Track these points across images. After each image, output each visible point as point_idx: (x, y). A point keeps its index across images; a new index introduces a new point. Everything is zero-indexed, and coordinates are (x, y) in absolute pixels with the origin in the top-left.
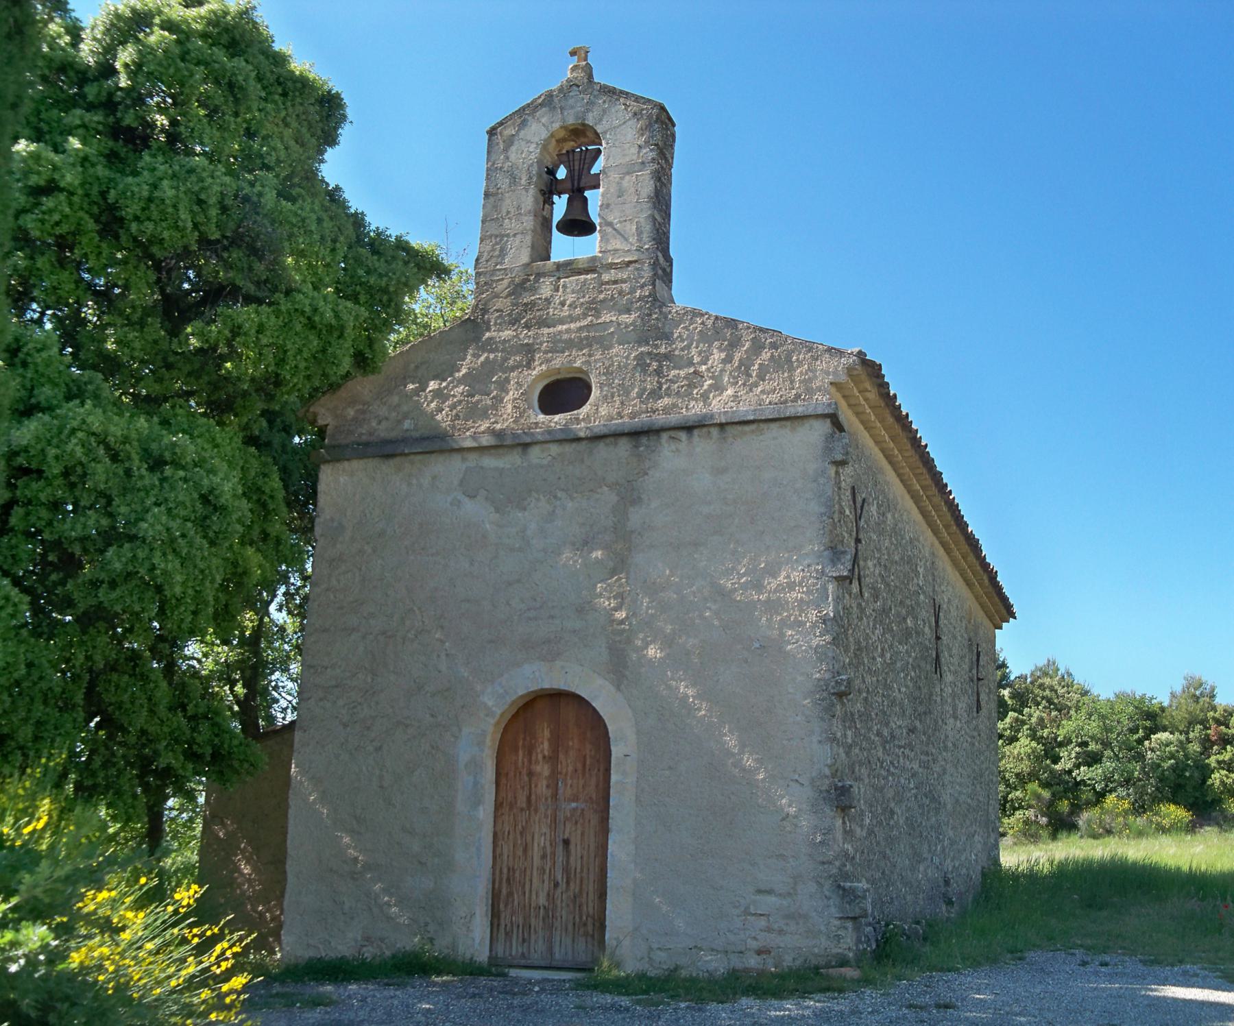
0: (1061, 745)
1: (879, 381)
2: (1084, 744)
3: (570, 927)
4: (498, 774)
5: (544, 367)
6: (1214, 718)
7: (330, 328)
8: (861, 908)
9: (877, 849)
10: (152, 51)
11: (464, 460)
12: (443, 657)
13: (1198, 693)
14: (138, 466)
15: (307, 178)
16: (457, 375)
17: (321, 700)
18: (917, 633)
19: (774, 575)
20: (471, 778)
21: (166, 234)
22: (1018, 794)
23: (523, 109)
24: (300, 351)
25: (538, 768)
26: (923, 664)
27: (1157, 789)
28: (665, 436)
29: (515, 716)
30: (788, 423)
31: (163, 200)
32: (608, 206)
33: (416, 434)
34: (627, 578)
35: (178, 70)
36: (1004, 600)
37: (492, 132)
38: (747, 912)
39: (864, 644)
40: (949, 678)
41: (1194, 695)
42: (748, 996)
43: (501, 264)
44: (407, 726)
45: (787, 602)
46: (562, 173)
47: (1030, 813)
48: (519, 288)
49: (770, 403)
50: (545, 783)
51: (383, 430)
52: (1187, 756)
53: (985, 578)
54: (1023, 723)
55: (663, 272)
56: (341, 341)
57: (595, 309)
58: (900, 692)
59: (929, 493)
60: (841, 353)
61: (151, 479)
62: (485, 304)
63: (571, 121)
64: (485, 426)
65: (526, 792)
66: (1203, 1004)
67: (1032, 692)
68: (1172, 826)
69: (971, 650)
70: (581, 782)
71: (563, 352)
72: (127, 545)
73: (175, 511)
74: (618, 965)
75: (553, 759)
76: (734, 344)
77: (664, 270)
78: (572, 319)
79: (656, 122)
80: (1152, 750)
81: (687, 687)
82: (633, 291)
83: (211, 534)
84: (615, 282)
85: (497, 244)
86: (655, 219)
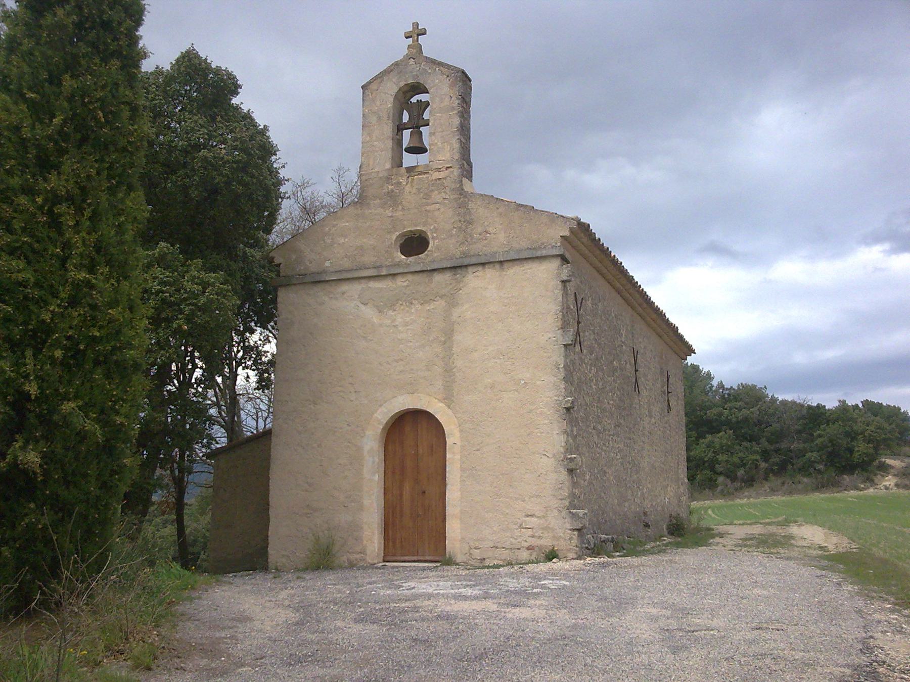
40: (644, 393)
46: (406, 117)
55: (467, 171)
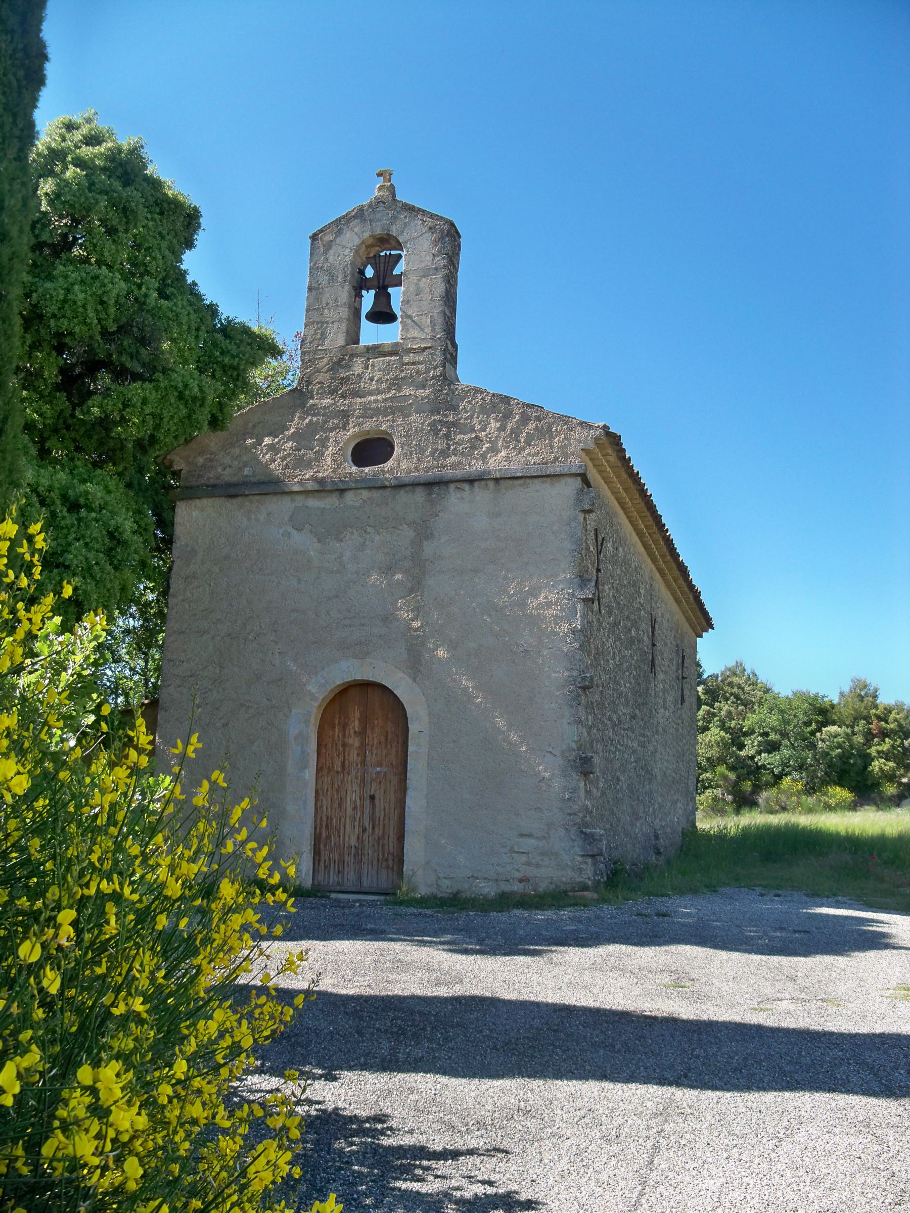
0: (746, 734)
1: (618, 448)
2: (766, 734)
3: (375, 863)
4: (319, 745)
5: (356, 429)
6: (876, 715)
7: (194, 399)
8: (598, 848)
9: (607, 806)
10: (67, 183)
11: (293, 500)
12: (277, 654)
13: (863, 694)
14: (61, 510)
15: (177, 279)
16: (286, 433)
17: (179, 686)
18: (639, 641)
19: (536, 596)
20: (299, 748)
21: (77, 329)
22: (708, 775)
23: (339, 219)
24: (172, 417)
25: (351, 741)
26: (642, 666)
27: (826, 773)
28: (452, 486)
29: (332, 701)
30: (549, 479)
31: (75, 302)
32: (408, 302)
33: (253, 480)
34: (422, 596)
35: (87, 199)
36: (705, 614)
37: (314, 238)
38: (512, 851)
39: (601, 650)
40: (661, 676)
41: (860, 695)
42: (518, 908)
43: (322, 345)
44: (248, 707)
45: (545, 617)
46: (369, 272)
47: (718, 792)
48: (337, 365)
49: (534, 463)
50: (356, 752)
51: (227, 476)
52: (852, 747)
53: (691, 596)
54: (714, 715)
55: (450, 357)
56: (203, 409)
57: (397, 384)
58: (625, 687)
59: (651, 531)
60: (590, 427)
61: (70, 519)
62: (309, 378)
63: (378, 231)
64: (309, 474)
65: (341, 759)
66: (847, 918)
67: (722, 689)
68: (837, 805)
69: (677, 654)
70: (385, 752)
71: (372, 418)
72: (55, 571)
73: (92, 545)
74: (414, 889)
75: (362, 734)
76: (507, 416)
77: (451, 355)
78: (379, 392)
79: (447, 235)
80: (823, 741)
81: (467, 680)
82: (427, 371)
83: (116, 562)
84: (414, 363)
85: (318, 329)
86: (445, 314)
